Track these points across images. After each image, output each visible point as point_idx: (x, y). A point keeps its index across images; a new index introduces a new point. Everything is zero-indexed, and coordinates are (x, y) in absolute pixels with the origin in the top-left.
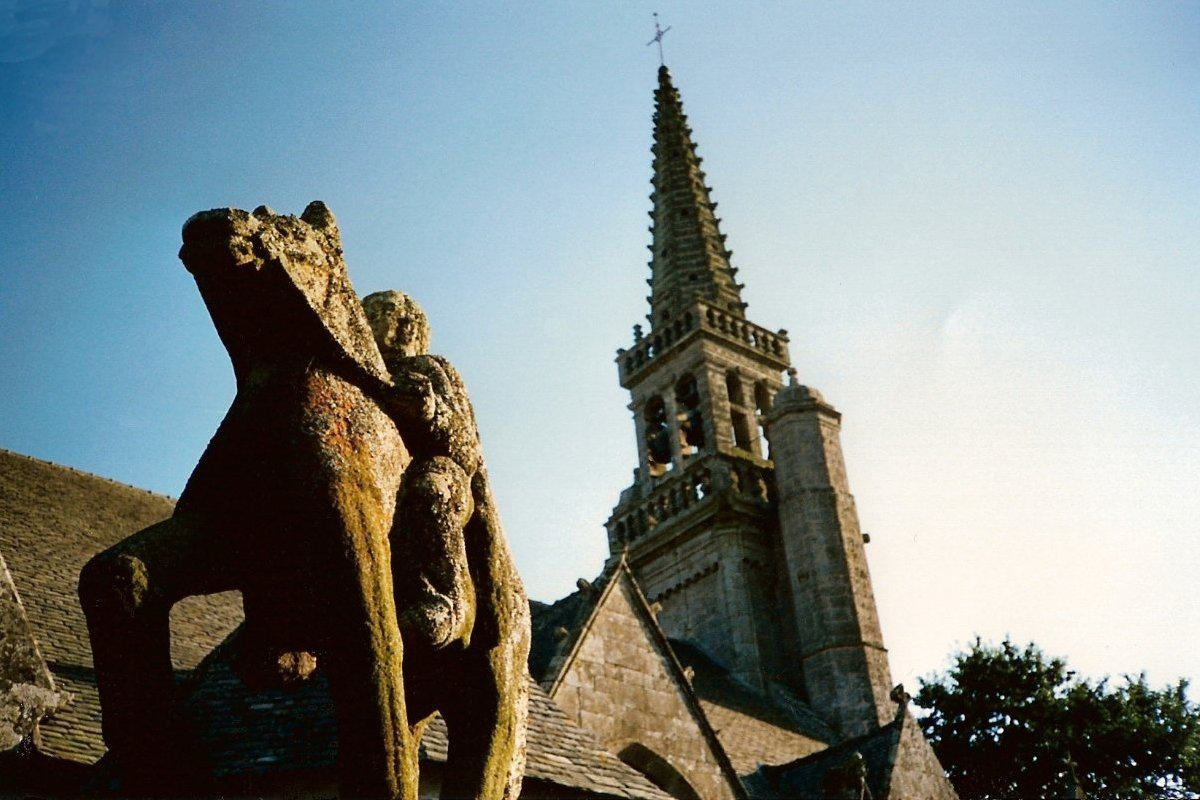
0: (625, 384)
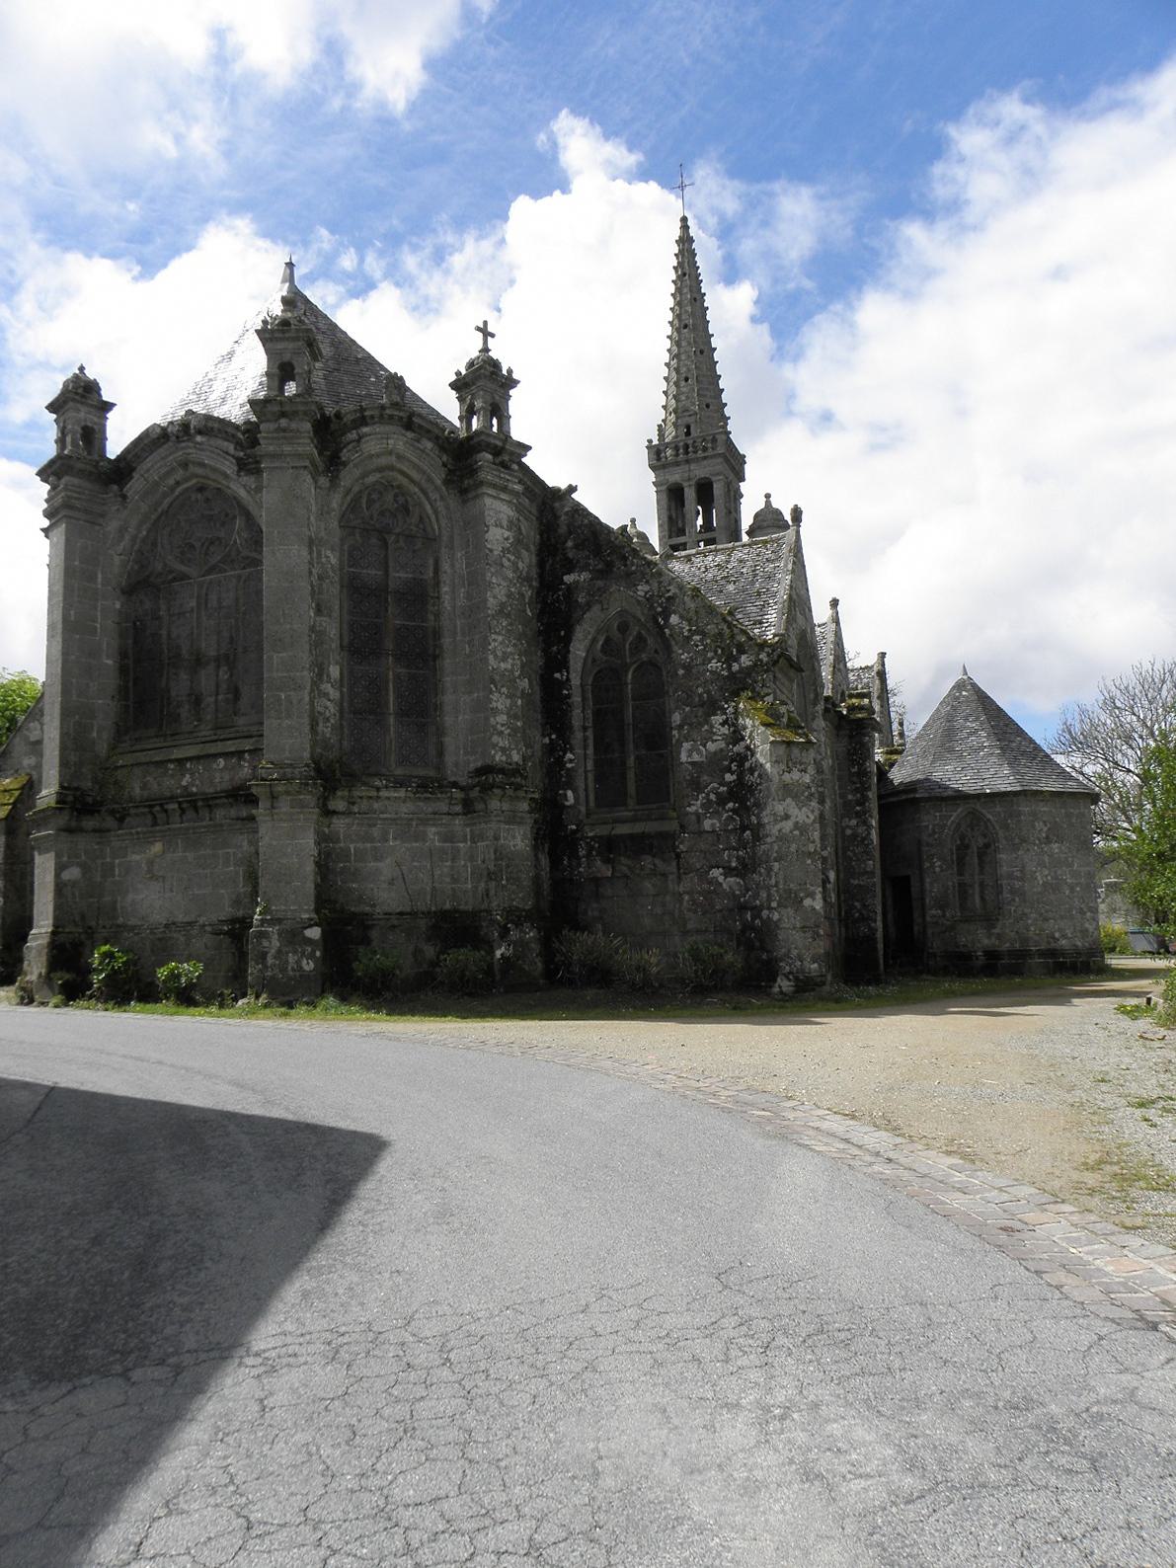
0: (652, 467)
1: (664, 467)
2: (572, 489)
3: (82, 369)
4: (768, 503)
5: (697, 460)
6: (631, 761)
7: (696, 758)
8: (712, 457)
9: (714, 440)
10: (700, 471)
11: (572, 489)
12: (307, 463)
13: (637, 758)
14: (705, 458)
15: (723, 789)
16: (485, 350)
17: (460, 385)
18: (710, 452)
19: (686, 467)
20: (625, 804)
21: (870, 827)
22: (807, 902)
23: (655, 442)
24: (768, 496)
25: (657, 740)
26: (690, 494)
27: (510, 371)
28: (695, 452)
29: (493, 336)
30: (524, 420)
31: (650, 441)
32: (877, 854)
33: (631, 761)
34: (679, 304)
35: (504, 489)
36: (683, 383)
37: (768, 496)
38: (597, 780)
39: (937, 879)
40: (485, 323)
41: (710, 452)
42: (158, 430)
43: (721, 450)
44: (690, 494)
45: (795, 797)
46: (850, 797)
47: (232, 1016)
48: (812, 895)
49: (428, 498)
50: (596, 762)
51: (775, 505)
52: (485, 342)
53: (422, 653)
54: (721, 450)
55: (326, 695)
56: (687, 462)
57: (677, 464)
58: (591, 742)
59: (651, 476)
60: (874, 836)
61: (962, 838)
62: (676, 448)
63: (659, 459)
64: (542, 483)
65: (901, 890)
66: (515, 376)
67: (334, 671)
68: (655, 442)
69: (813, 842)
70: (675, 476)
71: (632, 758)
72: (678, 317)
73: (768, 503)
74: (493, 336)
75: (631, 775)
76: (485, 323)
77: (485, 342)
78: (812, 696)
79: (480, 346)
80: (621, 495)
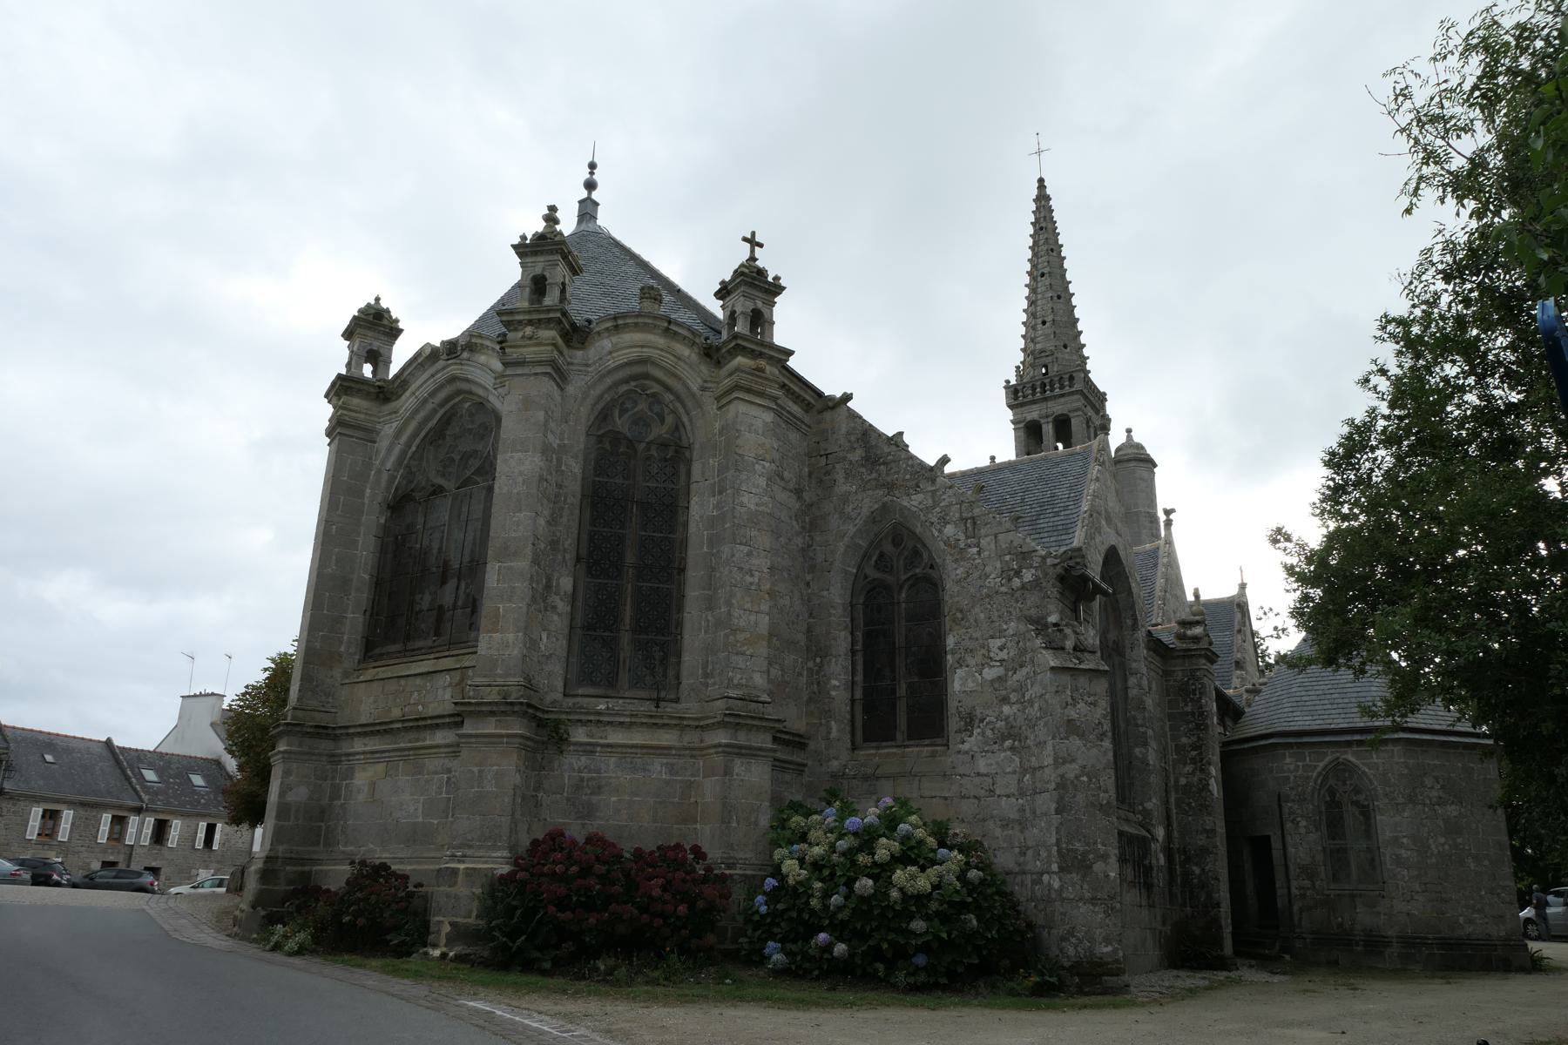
0: (1011, 407)
1: (1022, 405)
2: (847, 397)
3: (377, 299)
4: (1129, 437)
5: (1055, 397)
6: (902, 690)
7: (971, 685)
8: (1072, 393)
9: (1071, 378)
10: (1057, 408)
11: (847, 397)
12: (549, 370)
13: (910, 686)
14: (1062, 395)
15: (1000, 724)
16: (753, 259)
17: (723, 292)
18: (1067, 389)
19: (1044, 405)
20: (893, 739)
21: (1209, 775)
22: (1098, 867)
23: (1013, 382)
24: (1129, 431)
25: (932, 666)
26: (1048, 430)
27: (777, 278)
28: (1052, 390)
29: (761, 246)
30: (789, 325)
31: (1008, 382)
32: (1219, 809)
33: (902, 690)
34: (1035, 255)
35: (761, 394)
36: (1040, 326)
37: (1129, 431)
38: (865, 711)
39: (1301, 844)
40: (753, 234)
41: (1067, 389)
42: (428, 351)
43: (1077, 387)
44: (1048, 430)
45: (1082, 735)
46: (1184, 740)
47: (417, 975)
48: (1104, 857)
49: (684, 406)
50: (865, 689)
51: (1137, 439)
52: (752, 251)
53: (664, 566)
54: (1077, 387)
55: (554, 608)
56: (1045, 399)
57: (1033, 402)
58: (860, 668)
59: (1009, 414)
60: (1215, 787)
61: (1332, 792)
62: (1034, 388)
63: (1016, 398)
64: (819, 394)
65: (1253, 850)
66: (783, 282)
67: (566, 583)
68: (1013, 382)
69: (1106, 791)
70: (1033, 413)
71: (904, 686)
72: (1034, 266)
73: (1129, 437)
74: (761, 246)
75: (902, 707)
76: (753, 234)
77: (752, 251)
78: (1129, 622)
79: (747, 256)
80: (961, 427)
